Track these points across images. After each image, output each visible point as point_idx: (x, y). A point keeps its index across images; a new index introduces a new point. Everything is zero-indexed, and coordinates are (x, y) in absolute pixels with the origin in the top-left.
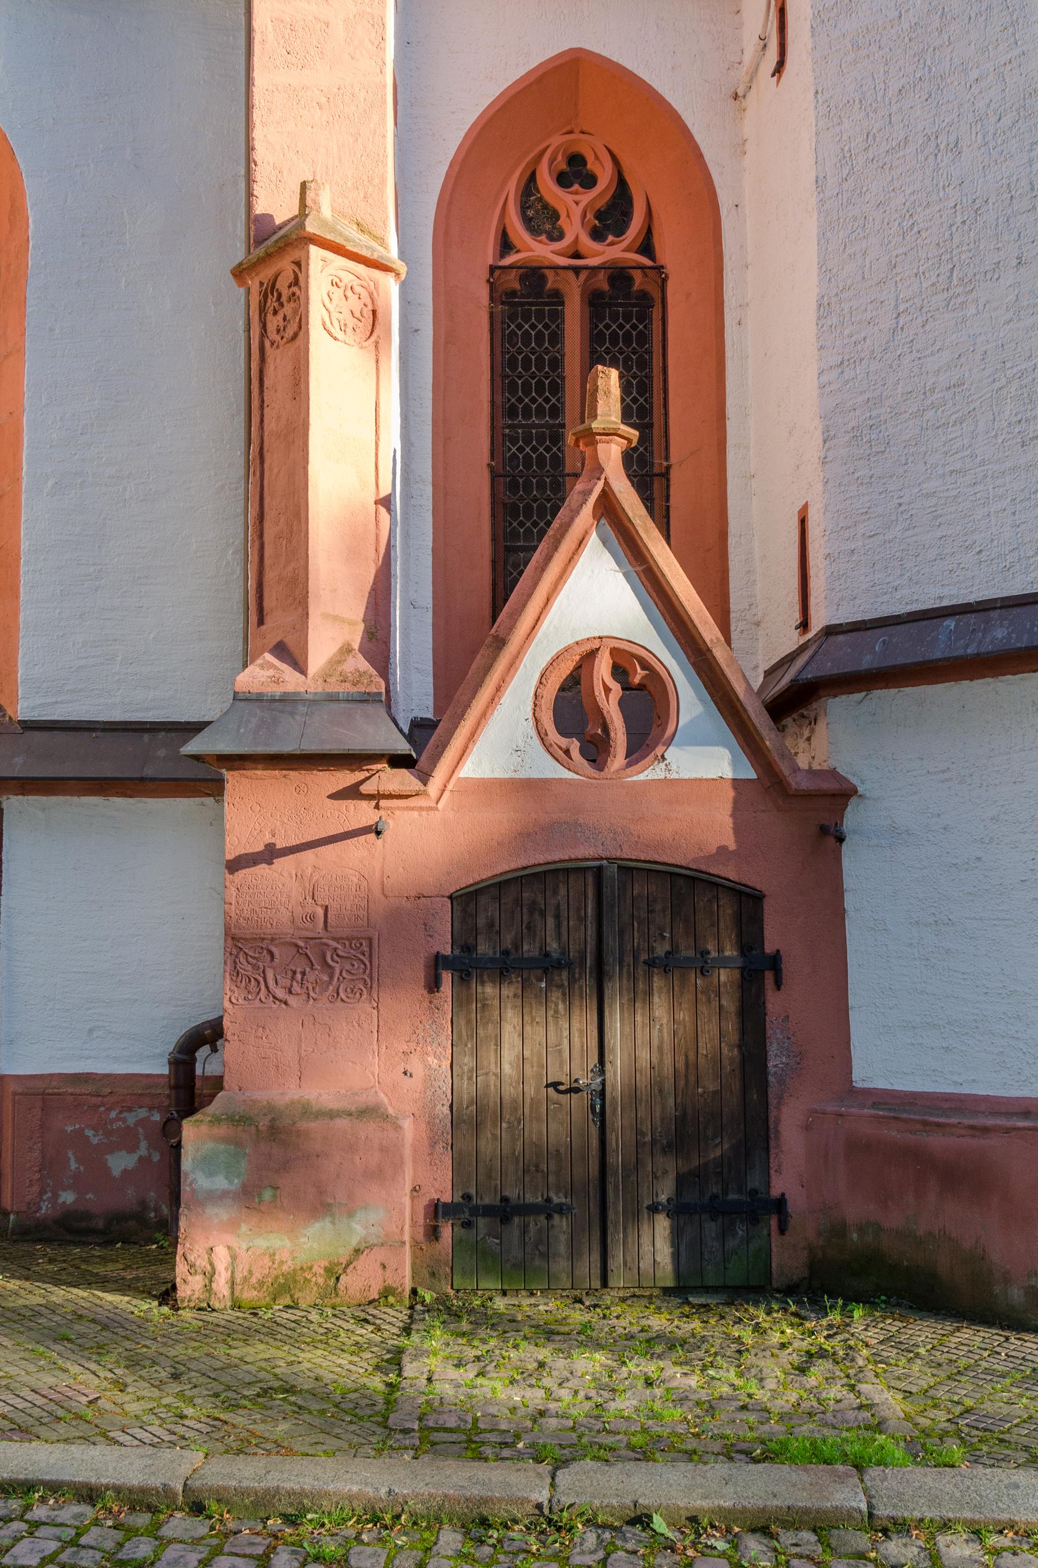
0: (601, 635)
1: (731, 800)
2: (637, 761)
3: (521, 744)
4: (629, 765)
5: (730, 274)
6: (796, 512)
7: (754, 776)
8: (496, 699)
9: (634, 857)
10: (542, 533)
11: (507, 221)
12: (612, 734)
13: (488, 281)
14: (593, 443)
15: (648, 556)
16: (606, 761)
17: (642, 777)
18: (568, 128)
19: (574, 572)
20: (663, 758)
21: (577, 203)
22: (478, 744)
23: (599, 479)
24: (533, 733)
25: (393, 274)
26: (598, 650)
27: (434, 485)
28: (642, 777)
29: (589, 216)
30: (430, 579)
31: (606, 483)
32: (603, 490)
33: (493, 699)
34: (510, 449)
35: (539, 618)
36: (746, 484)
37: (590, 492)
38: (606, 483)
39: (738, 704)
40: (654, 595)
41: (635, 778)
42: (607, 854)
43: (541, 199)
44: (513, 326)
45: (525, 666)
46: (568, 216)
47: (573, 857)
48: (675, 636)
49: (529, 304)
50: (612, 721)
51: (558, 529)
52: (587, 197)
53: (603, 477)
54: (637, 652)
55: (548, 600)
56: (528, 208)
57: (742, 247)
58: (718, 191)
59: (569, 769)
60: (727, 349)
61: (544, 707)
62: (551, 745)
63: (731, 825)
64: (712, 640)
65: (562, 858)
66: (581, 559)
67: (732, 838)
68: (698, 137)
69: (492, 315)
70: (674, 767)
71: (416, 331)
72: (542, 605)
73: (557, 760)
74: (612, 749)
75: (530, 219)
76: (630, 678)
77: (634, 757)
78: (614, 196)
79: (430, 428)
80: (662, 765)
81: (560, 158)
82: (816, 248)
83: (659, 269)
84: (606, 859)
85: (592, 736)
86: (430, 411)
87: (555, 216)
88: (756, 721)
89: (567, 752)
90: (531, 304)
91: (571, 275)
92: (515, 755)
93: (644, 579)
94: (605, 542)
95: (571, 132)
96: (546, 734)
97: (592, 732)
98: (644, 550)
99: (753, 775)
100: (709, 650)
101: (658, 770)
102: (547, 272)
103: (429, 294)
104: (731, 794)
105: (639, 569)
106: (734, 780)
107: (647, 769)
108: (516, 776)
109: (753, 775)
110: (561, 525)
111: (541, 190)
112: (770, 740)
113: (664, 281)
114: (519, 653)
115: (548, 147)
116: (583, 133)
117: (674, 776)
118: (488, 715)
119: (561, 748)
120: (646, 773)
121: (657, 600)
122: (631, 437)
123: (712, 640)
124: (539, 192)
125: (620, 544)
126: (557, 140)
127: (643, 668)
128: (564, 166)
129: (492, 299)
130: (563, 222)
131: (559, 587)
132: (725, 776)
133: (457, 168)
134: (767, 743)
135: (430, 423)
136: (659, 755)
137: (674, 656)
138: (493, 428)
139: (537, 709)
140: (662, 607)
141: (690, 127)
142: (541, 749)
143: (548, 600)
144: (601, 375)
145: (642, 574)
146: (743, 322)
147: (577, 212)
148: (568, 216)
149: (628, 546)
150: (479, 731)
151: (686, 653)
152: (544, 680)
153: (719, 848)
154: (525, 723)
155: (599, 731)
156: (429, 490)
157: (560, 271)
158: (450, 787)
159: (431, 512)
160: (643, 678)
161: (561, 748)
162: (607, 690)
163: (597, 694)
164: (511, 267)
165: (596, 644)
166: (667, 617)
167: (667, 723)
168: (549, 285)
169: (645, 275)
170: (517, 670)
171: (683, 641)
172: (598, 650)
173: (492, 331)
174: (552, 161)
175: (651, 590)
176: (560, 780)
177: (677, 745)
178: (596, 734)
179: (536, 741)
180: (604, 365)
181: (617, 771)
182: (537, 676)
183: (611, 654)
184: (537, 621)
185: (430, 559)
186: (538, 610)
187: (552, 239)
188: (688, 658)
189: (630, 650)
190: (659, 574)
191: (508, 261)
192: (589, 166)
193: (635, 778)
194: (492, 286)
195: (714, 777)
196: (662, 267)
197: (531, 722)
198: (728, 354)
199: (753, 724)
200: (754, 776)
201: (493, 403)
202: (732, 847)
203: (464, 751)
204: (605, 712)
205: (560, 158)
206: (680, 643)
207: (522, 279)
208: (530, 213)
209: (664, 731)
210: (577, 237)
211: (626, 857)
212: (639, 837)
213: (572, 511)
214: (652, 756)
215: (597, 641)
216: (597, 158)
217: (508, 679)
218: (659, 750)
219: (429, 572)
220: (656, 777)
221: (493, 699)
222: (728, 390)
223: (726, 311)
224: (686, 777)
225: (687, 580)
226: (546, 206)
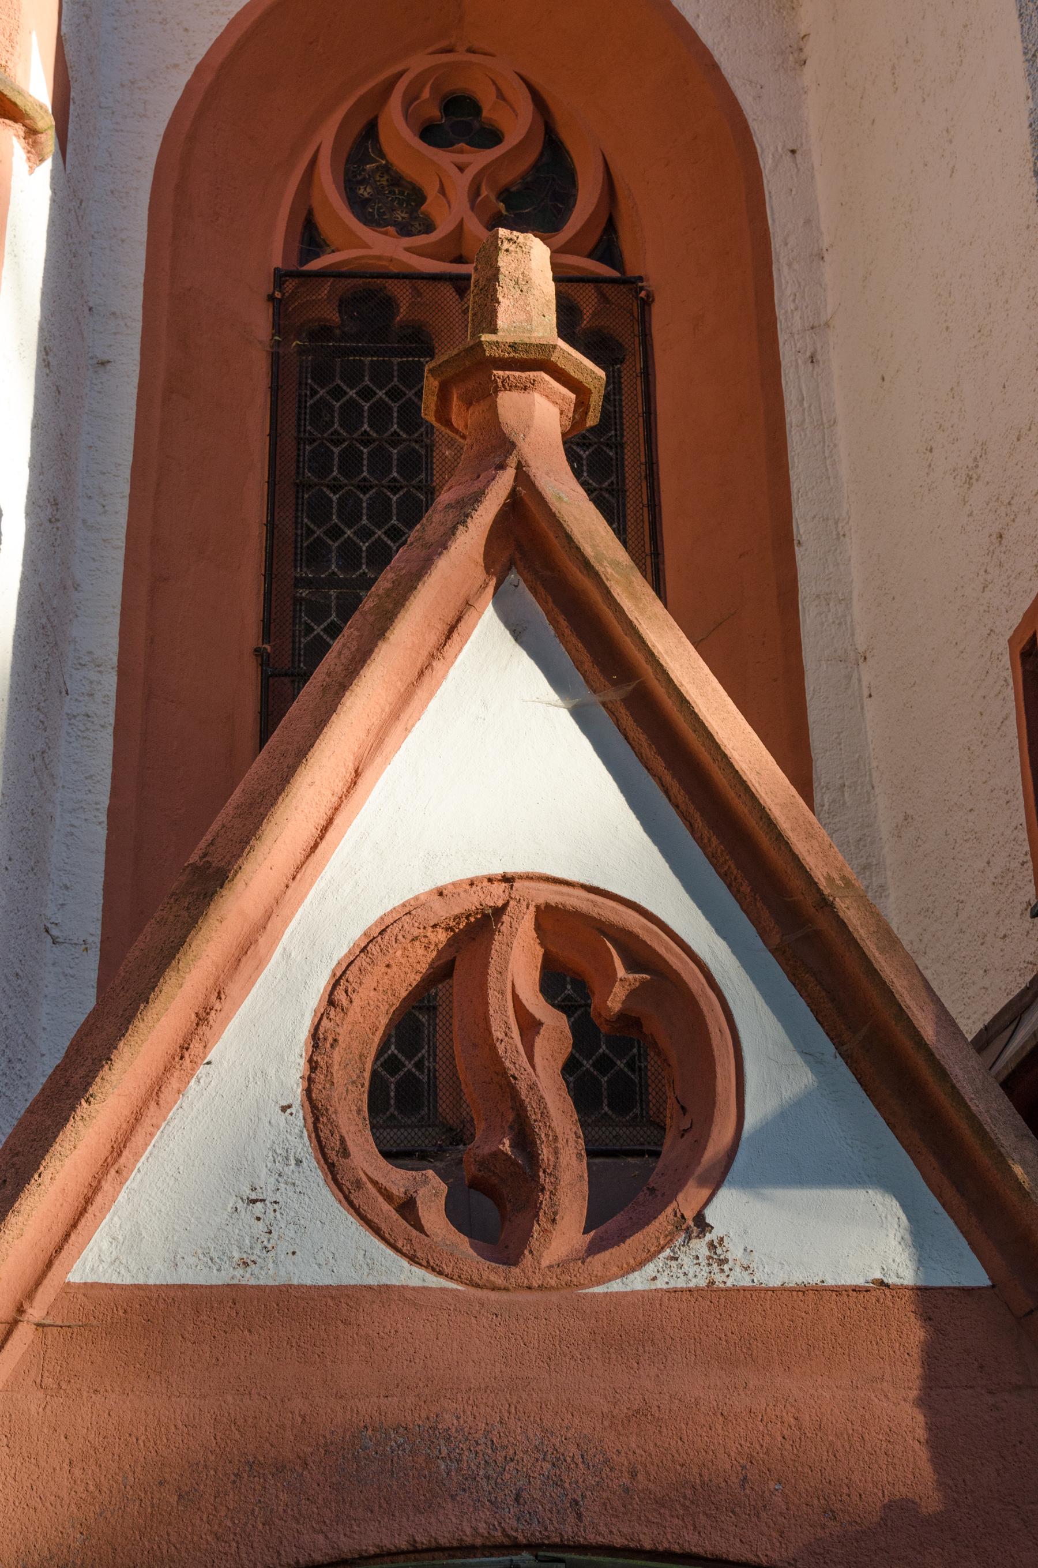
0: (511, 869)
1: (916, 1353)
2: (621, 1237)
3: (266, 1183)
4: (594, 1248)
5: (785, 270)
6: (1001, 647)
7: (984, 1281)
8: (196, 1046)
9: (619, 1541)
10: (347, 610)
11: (316, 202)
12: (545, 1153)
13: (271, 298)
14: (488, 393)
15: (639, 657)
16: (529, 1233)
17: (638, 1282)
18: (444, 44)
19: (433, 704)
20: (702, 1225)
21: (461, 169)
22: (133, 1182)
23: (502, 467)
24: (303, 1147)
25: (19, 128)
26: (499, 912)
27: (123, 672)
28: (638, 1282)
29: (485, 192)
30: (99, 878)
31: (519, 467)
32: (513, 493)
33: (185, 1047)
34: (309, 630)
35: (330, 821)
36: (849, 677)
37: (477, 498)
38: (523, 476)
39: (919, 1060)
40: (659, 765)
41: (616, 1286)
42: (534, 1531)
43: (387, 169)
44: (322, 392)
45: (287, 955)
46: (442, 191)
47: (422, 1540)
48: (724, 876)
49: (355, 351)
50: (545, 1113)
51: (388, 592)
52: (480, 159)
53: (512, 461)
54: (614, 918)
55: (357, 773)
56: (361, 182)
57: (808, 222)
58: (754, 126)
59: (413, 1259)
60: (788, 407)
61: (338, 1074)
62: (358, 1184)
63: (921, 1433)
64: (830, 879)
65: (388, 1543)
66: (452, 672)
67: (927, 1471)
68: (707, 38)
69: (275, 359)
70: (734, 1251)
71: (103, 364)
72: (339, 787)
73: (377, 1231)
74: (545, 1198)
75: (365, 202)
76: (595, 1001)
77: (611, 1225)
78: (536, 167)
79: (121, 554)
80: (700, 1246)
81: (426, 94)
82: (1016, 24)
83: (631, 283)
84: (530, 1547)
85: (482, 1163)
86: (123, 520)
87: (417, 196)
88: (978, 1106)
89: (407, 1208)
90: (363, 352)
91: (448, 291)
92: (246, 1215)
93: (628, 721)
94: (519, 632)
95: (449, 50)
96: (345, 1153)
97: (486, 1150)
98: (628, 642)
99: (975, 1275)
100: (825, 904)
101: (686, 1260)
102: (393, 287)
103: (137, 297)
104: (916, 1334)
105: (613, 695)
106: (921, 1291)
107: (651, 1257)
108: (247, 1278)
109: (975, 1275)
110: (397, 584)
111: (386, 148)
112: (1023, 1163)
113: (646, 303)
114: (268, 916)
115: (400, 75)
116: (471, 51)
117: (738, 1278)
118: (166, 1095)
119: (388, 1196)
120: (650, 1269)
121: (668, 778)
122: (588, 382)
123: (830, 879)
124: (383, 156)
125: (560, 635)
126: (418, 63)
127: (632, 965)
128: (434, 112)
129: (277, 327)
130: (432, 206)
131: (390, 741)
132: (891, 1280)
133: (209, 78)
134: (1018, 1170)
135: (122, 543)
136: (690, 1214)
137: (721, 928)
138: (270, 574)
139: (319, 1077)
140: (681, 797)
141: (690, 18)
142: (326, 1197)
143: (357, 773)
144: (506, 245)
145: (623, 712)
146: (819, 357)
147: (460, 184)
148: (442, 191)
149: (581, 636)
150: (138, 1139)
151: (756, 922)
152: (340, 996)
153: (888, 1507)
154: (282, 1117)
155: (506, 1146)
156: (110, 682)
157: (420, 284)
158: (36, 1312)
159: (110, 730)
160: (632, 994)
161: (388, 1196)
162: (529, 1026)
163: (498, 1033)
164: (322, 274)
165: (497, 894)
166: (699, 822)
167: (708, 1120)
168: (403, 312)
169: (603, 297)
170: (259, 967)
171: (746, 888)
172: (499, 912)
173: (275, 390)
174: (410, 99)
175: (649, 752)
176: (384, 1290)
177: (747, 1184)
178: (497, 1154)
179: (313, 1174)
180: (511, 228)
181: (562, 1265)
182: (321, 983)
183: (538, 927)
184: (325, 829)
185: (102, 832)
186: (327, 801)
187: (405, 230)
188: (763, 933)
189: (594, 912)
190: (669, 704)
191: (315, 265)
192: (485, 114)
193: (616, 1286)
194: (278, 306)
195: (860, 1281)
196: (641, 279)
197: (298, 1117)
198: (792, 417)
199: (972, 1118)
200: (984, 1281)
201: (271, 527)
202: (932, 1502)
203: (88, 1201)
204: (522, 1087)
205: (426, 94)
206: (737, 894)
207: (344, 304)
208: (365, 192)
209: (700, 1145)
210: (461, 224)
211: (593, 1538)
212: (633, 1474)
213: (427, 546)
214: (664, 1220)
215: (499, 888)
216: (501, 95)
217: (233, 989)
218: (688, 1201)
219: (99, 861)
220: (681, 1283)
221: (185, 1047)
222: (794, 487)
223: (782, 337)
224: (775, 1282)
225: (749, 729)
226: (397, 180)
